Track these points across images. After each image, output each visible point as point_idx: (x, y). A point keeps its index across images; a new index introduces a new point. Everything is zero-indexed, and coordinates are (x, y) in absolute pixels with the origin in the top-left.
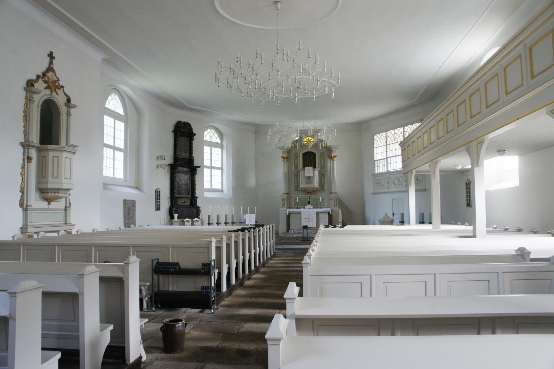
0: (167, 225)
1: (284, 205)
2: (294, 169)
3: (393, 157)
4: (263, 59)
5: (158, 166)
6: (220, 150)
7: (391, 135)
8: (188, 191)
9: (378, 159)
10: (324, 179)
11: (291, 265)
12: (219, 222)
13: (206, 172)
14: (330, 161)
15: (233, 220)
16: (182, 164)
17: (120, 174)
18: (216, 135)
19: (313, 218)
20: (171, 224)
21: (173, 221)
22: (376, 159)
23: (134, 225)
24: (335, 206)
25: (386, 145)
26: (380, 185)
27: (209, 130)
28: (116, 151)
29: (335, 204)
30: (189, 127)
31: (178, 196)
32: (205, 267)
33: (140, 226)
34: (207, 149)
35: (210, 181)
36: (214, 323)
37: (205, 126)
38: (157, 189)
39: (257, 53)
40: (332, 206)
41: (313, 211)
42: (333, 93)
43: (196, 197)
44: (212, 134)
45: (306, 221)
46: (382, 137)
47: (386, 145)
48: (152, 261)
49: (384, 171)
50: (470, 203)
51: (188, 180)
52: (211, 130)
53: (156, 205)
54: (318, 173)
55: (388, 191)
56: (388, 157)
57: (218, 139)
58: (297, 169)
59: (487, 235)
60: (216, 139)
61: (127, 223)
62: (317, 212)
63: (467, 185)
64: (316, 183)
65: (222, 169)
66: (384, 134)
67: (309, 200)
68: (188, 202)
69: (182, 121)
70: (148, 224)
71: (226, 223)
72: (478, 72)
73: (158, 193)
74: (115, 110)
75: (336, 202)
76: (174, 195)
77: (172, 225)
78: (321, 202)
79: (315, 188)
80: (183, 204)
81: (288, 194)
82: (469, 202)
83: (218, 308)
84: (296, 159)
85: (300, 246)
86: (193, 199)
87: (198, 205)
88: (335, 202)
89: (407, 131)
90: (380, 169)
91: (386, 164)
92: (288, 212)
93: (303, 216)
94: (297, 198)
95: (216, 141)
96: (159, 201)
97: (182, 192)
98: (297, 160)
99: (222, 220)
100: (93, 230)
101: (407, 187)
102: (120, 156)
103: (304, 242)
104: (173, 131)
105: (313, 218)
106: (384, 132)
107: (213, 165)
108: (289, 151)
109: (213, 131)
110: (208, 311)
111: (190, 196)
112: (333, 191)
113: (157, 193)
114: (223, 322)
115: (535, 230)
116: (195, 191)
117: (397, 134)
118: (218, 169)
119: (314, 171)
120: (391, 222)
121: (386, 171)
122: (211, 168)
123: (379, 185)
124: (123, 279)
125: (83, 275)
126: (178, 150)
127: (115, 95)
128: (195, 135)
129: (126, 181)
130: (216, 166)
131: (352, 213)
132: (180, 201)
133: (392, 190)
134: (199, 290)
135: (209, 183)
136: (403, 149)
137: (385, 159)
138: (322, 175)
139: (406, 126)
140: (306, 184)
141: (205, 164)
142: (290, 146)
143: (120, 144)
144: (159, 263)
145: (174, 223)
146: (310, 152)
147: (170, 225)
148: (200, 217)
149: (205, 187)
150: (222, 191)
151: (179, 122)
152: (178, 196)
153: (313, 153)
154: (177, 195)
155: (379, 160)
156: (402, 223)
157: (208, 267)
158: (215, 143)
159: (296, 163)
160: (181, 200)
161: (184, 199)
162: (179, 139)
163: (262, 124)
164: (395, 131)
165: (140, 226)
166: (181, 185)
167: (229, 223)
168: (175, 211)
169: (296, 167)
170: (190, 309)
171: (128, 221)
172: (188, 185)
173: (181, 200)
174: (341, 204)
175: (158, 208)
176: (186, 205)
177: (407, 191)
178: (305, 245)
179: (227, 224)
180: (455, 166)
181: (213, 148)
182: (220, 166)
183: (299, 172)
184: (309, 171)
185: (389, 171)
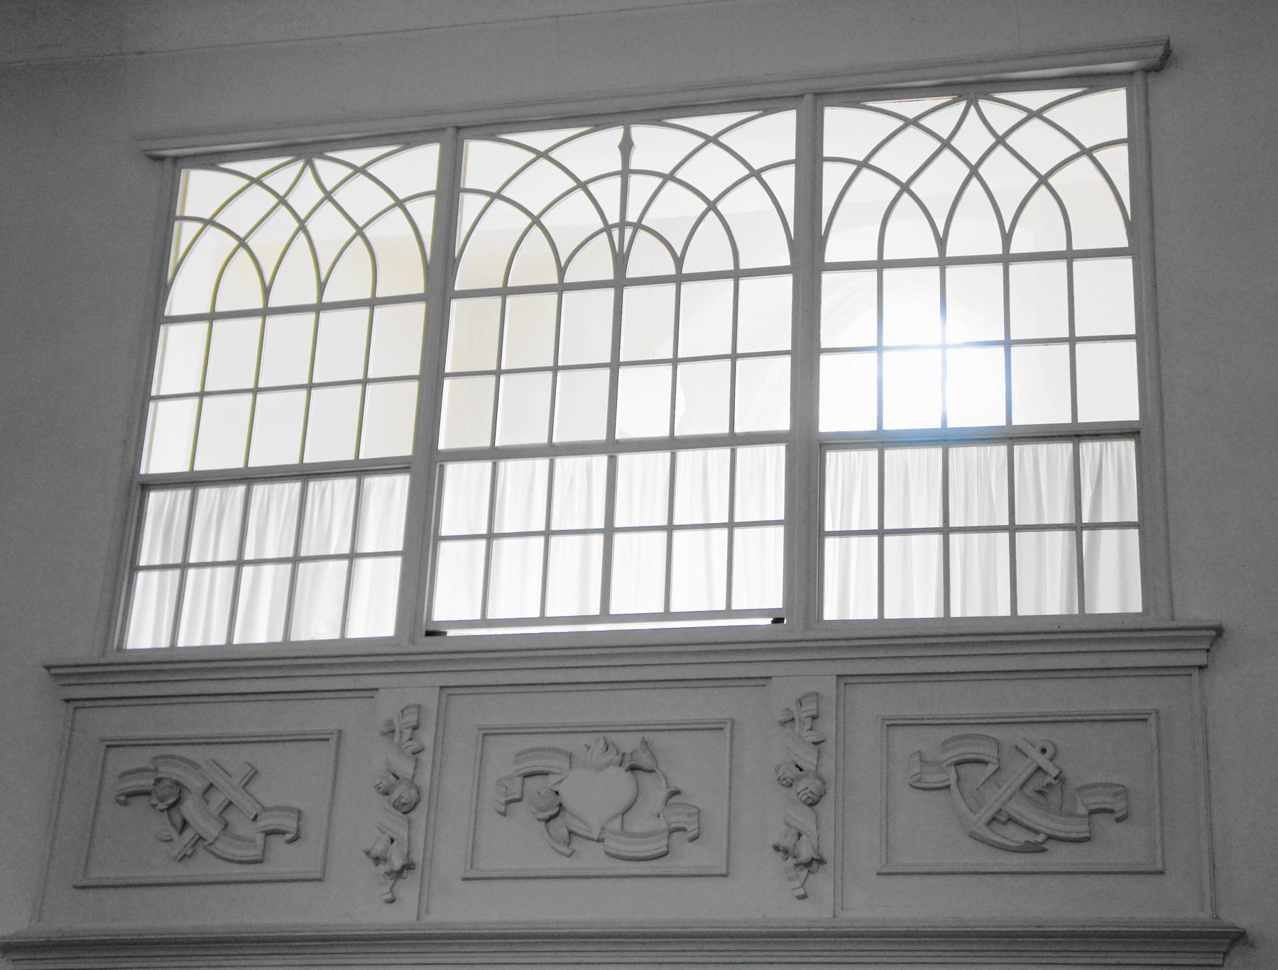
49: (359, 630)
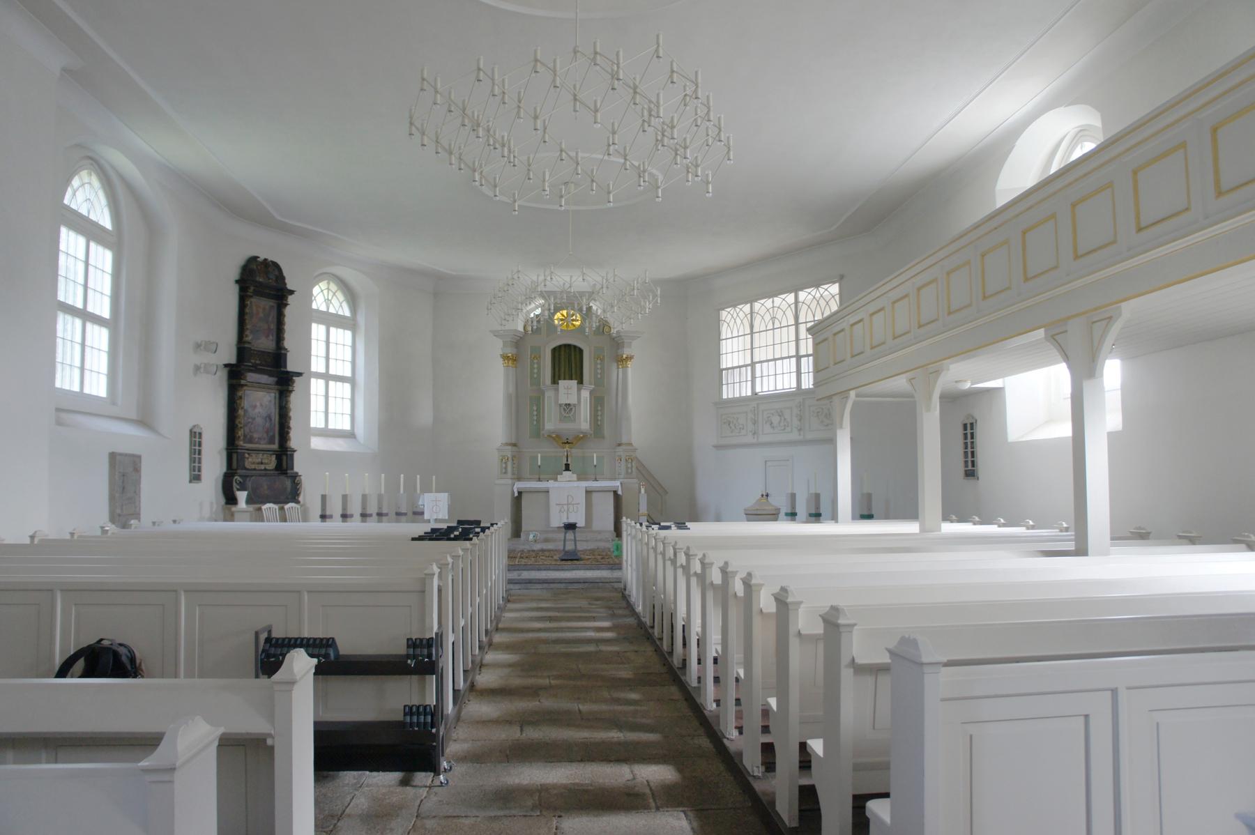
0: (216, 521)
1: (506, 473)
2: (531, 385)
3: (768, 361)
4: (558, 74)
5: (197, 369)
6: (348, 334)
7: (763, 311)
8: (271, 434)
9: (729, 365)
10: (602, 410)
11: (564, 624)
12: (328, 513)
13: (317, 386)
14: (618, 368)
15: (380, 508)
16: (258, 365)
17: (98, 387)
18: (340, 296)
19: (578, 504)
20: (230, 517)
21: (234, 509)
22: (724, 367)
23: (136, 519)
24: (628, 474)
25: (752, 333)
26: (735, 427)
27: (323, 285)
28: (89, 326)
29: (630, 471)
30: (277, 273)
31: (245, 445)
32: (418, 651)
33: (154, 523)
34: (318, 331)
35: (324, 410)
36: (467, 822)
37: (316, 274)
38: (194, 426)
39: (479, 69)
40: (622, 476)
41: (578, 487)
42: (710, 186)
43: (290, 448)
44: (331, 294)
45: (560, 511)
46: (741, 314)
47: (752, 333)
48: (257, 634)
49: (744, 394)
50: (974, 470)
51: (273, 407)
52: (328, 283)
53: (192, 469)
54: (588, 396)
55: (755, 441)
56: (756, 359)
57: (345, 305)
58: (540, 385)
59: (1112, 545)
60: (341, 306)
61: (119, 515)
62: (588, 489)
63: (965, 429)
64: (583, 422)
65: (352, 381)
66: (747, 308)
67: (567, 461)
68: (272, 462)
69: (259, 257)
70: (174, 519)
71: (364, 516)
72: (1122, 137)
73: (196, 437)
74: (89, 213)
75: (632, 466)
76: (236, 442)
77: (232, 520)
78: (595, 466)
79: (582, 433)
80: (257, 467)
81: (515, 445)
82: (970, 468)
83: (451, 768)
84: (535, 361)
85: (562, 572)
86: (284, 455)
87: (296, 469)
88: (629, 465)
89: (757, 313)
90: (736, 388)
91: (749, 378)
92: (518, 489)
93: (554, 498)
94: (539, 455)
95: (340, 313)
96: (200, 459)
97: (256, 435)
98: (539, 364)
99: (355, 509)
100: (32, 537)
101: (802, 433)
102: (100, 337)
103: (569, 563)
104: (237, 282)
105: (578, 504)
106: (746, 303)
107: (332, 372)
108: (518, 342)
109: (333, 287)
110: (422, 778)
111: (275, 446)
112: (624, 440)
113: (195, 437)
114: (496, 818)
115: (1191, 533)
116: (288, 433)
117: (779, 308)
118: (343, 382)
119: (579, 390)
120: (773, 516)
121: (749, 393)
122: (327, 377)
123: (731, 428)
124: (269, 742)
125: (172, 770)
126: (247, 329)
127: (91, 175)
128: (292, 292)
129: (114, 403)
130: (340, 373)
131: (666, 492)
132: (250, 460)
133: (763, 439)
134: (399, 717)
135: (322, 416)
136: (818, 342)
137: (746, 366)
138: (598, 402)
139: (802, 289)
140: (560, 420)
141: (313, 369)
142: (521, 329)
143: (101, 306)
144: (274, 641)
145: (236, 515)
146: (568, 346)
147: (225, 520)
148: (301, 499)
149: (313, 425)
150: (350, 435)
151: (254, 259)
152: (245, 445)
153: (575, 347)
154: (244, 443)
155: (733, 368)
156: (816, 516)
157: (425, 652)
158: (336, 315)
159: (536, 371)
160: (254, 455)
161: (261, 455)
162: (251, 303)
163: (454, 273)
164: (773, 302)
165: (154, 523)
166: (254, 419)
167: (371, 515)
168: (238, 484)
169: (536, 381)
170: (368, 773)
171: (122, 509)
172: (271, 420)
173: (254, 455)
174: (644, 474)
175: (196, 477)
176: (265, 469)
177: (831, 441)
178: (574, 572)
179: (368, 519)
180: (956, 382)
181: (332, 330)
182: (348, 373)
183: (543, 393)
184: (568, 389)
185: (756, 394)
